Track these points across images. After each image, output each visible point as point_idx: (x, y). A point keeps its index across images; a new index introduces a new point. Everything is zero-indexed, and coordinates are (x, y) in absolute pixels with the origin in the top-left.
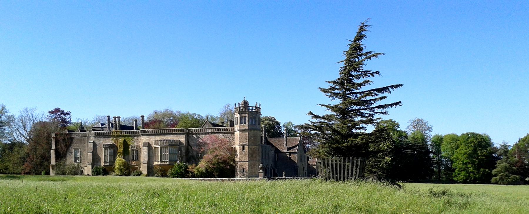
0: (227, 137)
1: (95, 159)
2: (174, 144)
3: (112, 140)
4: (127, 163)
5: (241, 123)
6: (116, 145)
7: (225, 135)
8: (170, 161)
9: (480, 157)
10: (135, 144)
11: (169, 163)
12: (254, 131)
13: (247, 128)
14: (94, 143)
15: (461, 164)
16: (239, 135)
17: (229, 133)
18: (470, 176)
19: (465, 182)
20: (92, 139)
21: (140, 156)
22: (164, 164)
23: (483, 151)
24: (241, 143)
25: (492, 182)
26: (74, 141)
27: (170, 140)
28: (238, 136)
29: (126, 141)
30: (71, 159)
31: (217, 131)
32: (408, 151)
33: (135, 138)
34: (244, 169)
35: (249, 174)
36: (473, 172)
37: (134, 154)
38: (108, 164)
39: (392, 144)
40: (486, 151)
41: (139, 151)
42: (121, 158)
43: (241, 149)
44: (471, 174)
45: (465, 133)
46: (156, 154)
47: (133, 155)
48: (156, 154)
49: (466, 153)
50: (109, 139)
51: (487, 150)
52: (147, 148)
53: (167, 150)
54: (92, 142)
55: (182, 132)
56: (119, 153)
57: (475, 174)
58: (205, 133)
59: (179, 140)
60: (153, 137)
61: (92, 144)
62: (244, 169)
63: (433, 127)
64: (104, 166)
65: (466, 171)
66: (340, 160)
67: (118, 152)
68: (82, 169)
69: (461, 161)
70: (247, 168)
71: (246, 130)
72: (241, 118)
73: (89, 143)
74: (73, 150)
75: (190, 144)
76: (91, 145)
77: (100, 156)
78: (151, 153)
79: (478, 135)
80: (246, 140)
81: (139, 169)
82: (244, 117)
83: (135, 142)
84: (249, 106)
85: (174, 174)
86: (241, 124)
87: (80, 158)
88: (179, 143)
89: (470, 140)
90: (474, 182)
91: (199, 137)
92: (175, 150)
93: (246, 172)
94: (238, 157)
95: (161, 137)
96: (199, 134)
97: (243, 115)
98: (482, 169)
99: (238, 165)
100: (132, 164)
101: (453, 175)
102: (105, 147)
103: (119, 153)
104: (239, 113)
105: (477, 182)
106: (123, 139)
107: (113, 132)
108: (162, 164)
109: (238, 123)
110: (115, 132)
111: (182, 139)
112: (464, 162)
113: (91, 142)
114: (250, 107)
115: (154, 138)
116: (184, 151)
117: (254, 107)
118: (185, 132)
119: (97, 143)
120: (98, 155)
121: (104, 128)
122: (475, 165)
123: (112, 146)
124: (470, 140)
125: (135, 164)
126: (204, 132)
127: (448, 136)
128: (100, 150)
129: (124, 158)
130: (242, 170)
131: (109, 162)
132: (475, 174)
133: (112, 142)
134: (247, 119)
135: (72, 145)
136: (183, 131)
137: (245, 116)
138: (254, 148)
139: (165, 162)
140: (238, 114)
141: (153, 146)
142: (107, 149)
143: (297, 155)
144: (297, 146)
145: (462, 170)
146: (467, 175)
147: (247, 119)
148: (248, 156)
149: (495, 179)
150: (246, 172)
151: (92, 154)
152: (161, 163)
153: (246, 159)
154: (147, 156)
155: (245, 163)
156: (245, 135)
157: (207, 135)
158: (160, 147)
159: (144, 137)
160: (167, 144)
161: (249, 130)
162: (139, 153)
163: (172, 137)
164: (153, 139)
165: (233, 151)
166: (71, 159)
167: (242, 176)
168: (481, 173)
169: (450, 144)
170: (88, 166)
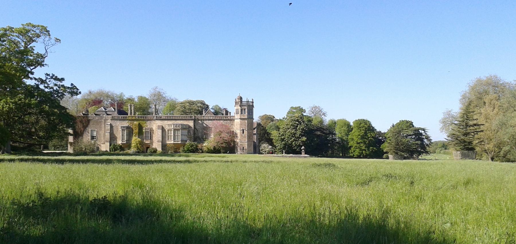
0: (227, 123)
1: (113, 138)
2: (184, 127)
3: (128, 122)
4: (142, 141)
5: (242, 113)
6: (131, 127)
7: (225, 121)
8: (182, 141)
9: (370, 138)
10: (148, 126)
11: (181, 142)
12: (251, 119)
13: (246, 117)
14: (111, 124)
15: (355, 143)
16: (239, 122)
17: (228, 120)
18: (363, 153)
19: (359, 157)
20: (109, 122)
21: (153, 136)
22: (176, 142)
23: (371, 134)
24: (242, 129)
25: (384, 158)
26: (91, 123)
27: (182, 125)
28: (239, 123)
29: (141, 124)
30: (88, 137)
31: (218, 119)
32: (318, 133)
33: (149, 122)
34: (243, 148)
35: (248, 151)
36: (365, 150)
37: (147, 134)
38: (125, 142)
39: (306, 127)
40: (374, 134)
41: (152, 132)
42: (137, 138)
43: (241, 133)
44: (364, 152)
45: (357, 119)
46: (169, 135)
47: (148, 135)
48: (169, 135)
49: (359, 135)
50: (125, 121)
51: (374, 133)
52: (161, 130)
53: (179, 132)
54: (109, 124)
55: (191, 118)
56: (134, 133)
57: (366, 151)
58: (209, 120)
59: (189, 125)
60: (166, 121)
61: (110, 125)
62: (243, 148)
63: (327, 113)
64: (122, 144)
65: (360, 149)
66: (466, 152)
67: (134, 133)
68: (99, 146)
69: (355, 141)
70: (246, 147)
71: (246, 119)
72: (242, 110)
73: (107, 124)
74: (90, 130)
75: (196, 128)
76: (108, 126)
77: (116, 135)
78: (164, 134)
79: (367, 122)
80: (245, 126)
81: (152, 146)
82: (244, 109)
83: (148, 125)
84: (243, 101)
85: (186, 151)
86: (241, 114)
87: (96, 137)
88: (189, 127)
89: (362, 125)
90: (365, 157)
91: (204, 123)
92: (186, 132)
93: (245, 150)
94: (239, 138)
95: (172, 122)
96: (204, 120)
97: (243, 108)
98: (371, 148)
99: (239, 145)
100: (146, 142)
101: (350, 152)
102: (122, 128)
103: (134, 133)
104: (240, 106)
105: (368, 157)
106: (137, 122)
107: (129, 117)
108: (175, 142)
109: (239, 113)
110: (130, 117)
111: (191, 124)
112: (358, 142)
113: (108, 124)
114: (243, 102)
115: (167, 123)
116: (192, 132)
117: (246, 102)
118: (194, 118)
119: (113, 125)
120: (114, 134)
121: (108, 112)
122: (366, 144)
123: (128, 128)
124: (362, 125)
125: (149, 142)
126: (208, 119)
127: (340, 120)
128: (116, 131)
129: (139, 137)
130: (242, 148)
131: (126, 141)
132: (366, 151)
133: (128, 124)
134: (246, 110)
135: (89, 126)
136: (192, 118)
137: (245, 108)
138: (251, 132)
139: (177, 141)
140: (239, 107)
141: (167, 128)
142: (125, 130)
143: (256, 136)
144: (255, 129)
145: (357, 148)
146: (361, 152)
147: (246, 110)
148: (247, 138)
149: (386, 155)
150: (245, 150)
151: (110, 134)
152: (174, 141)
153: (245, 140)
154: (161, 136)
155: (245, 143)
156: (245, 122)
157: (210, 121)
158: (174, 130)
159: (157, 121)
160: (179, 127)
161: (247, 118)
162: (152, 133)
163: (183, 122)
164: (166, 123)
165: (233, 135)
166: (88, 137)
167: (242, 153)
168: (371, 150)
169: (342, 127)
170: (106, 144)
